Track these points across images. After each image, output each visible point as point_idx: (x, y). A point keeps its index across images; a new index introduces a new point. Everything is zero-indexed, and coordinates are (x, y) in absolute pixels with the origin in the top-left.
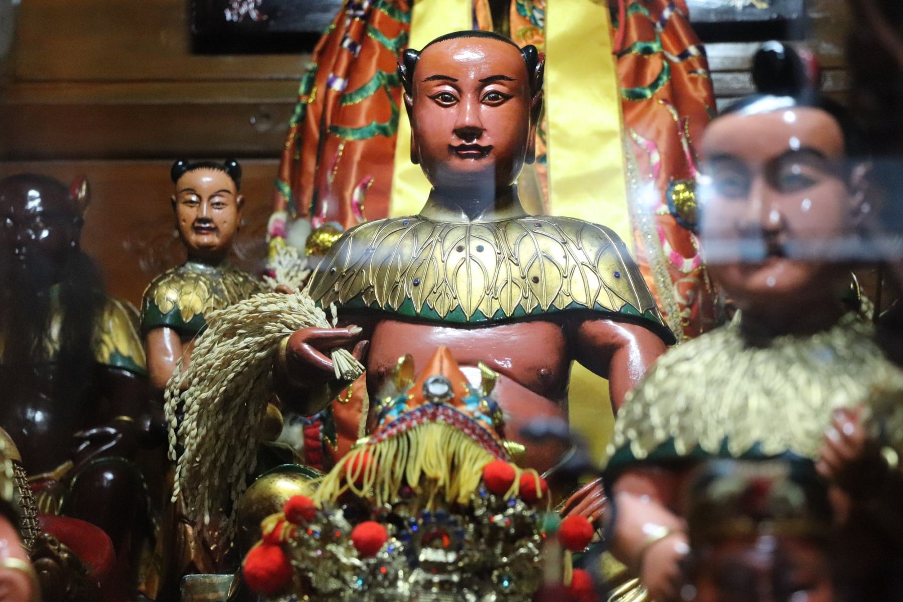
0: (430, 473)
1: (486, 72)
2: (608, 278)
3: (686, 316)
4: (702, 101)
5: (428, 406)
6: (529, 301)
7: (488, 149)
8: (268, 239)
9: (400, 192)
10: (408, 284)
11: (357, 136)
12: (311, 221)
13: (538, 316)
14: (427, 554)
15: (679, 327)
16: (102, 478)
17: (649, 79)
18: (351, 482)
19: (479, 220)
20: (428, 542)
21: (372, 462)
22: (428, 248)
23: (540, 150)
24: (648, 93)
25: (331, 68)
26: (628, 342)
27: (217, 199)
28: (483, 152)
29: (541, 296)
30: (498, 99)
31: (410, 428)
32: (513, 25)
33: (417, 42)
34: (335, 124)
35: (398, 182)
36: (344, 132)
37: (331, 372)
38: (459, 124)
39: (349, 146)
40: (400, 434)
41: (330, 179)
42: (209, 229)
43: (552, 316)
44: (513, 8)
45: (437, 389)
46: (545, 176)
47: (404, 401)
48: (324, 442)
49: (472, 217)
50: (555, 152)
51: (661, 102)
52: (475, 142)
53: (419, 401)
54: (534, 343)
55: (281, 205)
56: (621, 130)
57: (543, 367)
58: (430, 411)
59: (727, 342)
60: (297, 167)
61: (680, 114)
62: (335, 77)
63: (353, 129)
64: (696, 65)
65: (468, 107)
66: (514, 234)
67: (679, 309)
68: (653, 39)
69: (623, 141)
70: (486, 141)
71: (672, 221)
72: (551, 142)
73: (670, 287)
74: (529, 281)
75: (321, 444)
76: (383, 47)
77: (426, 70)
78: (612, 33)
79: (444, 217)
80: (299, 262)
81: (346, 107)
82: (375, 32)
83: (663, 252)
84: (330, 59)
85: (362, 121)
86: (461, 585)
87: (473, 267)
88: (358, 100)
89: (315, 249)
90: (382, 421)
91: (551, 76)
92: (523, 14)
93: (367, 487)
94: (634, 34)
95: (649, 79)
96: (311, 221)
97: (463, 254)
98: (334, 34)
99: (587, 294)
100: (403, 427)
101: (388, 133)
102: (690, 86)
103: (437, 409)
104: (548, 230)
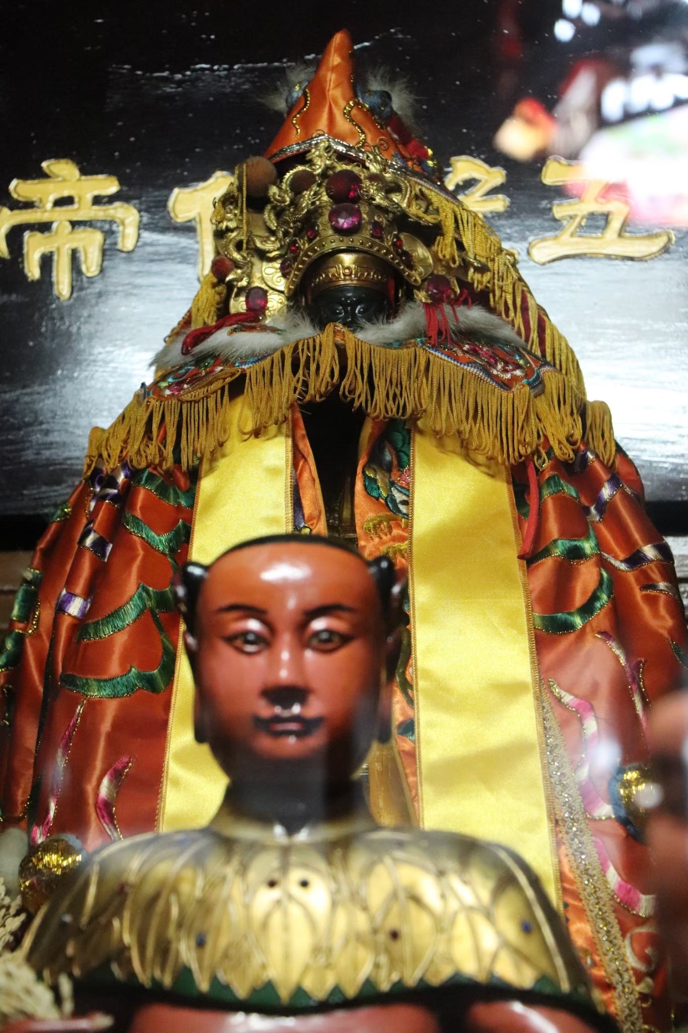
1: (314, 598)
2: (512, 931)
3: (646, 991)
4: (665, 633)
11: (107, 692)
12: (29, 832)
15: (635, 1010)
17: (579, 600)
19: (303, 836)
23: (403, 713)
24: (578, 621)
28: (306, 726)
33: (205, 547)
35: (173, 768)
38: (271, 680)
39: (94, 707)
44: (359, 486)
46: (412, 755)
49: (291, 830)
50: (428, 719)
52: (296, 709)
56: (534, 681)
61: (628, 654)
62: (71, 595)
63: (99, 681)
64: (656, 575)
66: (359, 859)
67: (633, 979)
68: (585, 535)
69: (538, 698)
70: (315, 708)
72: (421, 701)
73: (619, 941)
74: (382, 937)
76: (148, 546)
77: (219, 596)
78: (519, 524)
79: (247, 832)
80: (7, 900)
84: (63, 564)
85: (114, 668)
88: (107, 631)
91: (421, 594)
92: (375, 494)
94: (553, 527)
96: (29, 832)
97: (276, 893)
98: (69, 523)
101: (159, 685)
102: (646, 610)
104: (413, 854)
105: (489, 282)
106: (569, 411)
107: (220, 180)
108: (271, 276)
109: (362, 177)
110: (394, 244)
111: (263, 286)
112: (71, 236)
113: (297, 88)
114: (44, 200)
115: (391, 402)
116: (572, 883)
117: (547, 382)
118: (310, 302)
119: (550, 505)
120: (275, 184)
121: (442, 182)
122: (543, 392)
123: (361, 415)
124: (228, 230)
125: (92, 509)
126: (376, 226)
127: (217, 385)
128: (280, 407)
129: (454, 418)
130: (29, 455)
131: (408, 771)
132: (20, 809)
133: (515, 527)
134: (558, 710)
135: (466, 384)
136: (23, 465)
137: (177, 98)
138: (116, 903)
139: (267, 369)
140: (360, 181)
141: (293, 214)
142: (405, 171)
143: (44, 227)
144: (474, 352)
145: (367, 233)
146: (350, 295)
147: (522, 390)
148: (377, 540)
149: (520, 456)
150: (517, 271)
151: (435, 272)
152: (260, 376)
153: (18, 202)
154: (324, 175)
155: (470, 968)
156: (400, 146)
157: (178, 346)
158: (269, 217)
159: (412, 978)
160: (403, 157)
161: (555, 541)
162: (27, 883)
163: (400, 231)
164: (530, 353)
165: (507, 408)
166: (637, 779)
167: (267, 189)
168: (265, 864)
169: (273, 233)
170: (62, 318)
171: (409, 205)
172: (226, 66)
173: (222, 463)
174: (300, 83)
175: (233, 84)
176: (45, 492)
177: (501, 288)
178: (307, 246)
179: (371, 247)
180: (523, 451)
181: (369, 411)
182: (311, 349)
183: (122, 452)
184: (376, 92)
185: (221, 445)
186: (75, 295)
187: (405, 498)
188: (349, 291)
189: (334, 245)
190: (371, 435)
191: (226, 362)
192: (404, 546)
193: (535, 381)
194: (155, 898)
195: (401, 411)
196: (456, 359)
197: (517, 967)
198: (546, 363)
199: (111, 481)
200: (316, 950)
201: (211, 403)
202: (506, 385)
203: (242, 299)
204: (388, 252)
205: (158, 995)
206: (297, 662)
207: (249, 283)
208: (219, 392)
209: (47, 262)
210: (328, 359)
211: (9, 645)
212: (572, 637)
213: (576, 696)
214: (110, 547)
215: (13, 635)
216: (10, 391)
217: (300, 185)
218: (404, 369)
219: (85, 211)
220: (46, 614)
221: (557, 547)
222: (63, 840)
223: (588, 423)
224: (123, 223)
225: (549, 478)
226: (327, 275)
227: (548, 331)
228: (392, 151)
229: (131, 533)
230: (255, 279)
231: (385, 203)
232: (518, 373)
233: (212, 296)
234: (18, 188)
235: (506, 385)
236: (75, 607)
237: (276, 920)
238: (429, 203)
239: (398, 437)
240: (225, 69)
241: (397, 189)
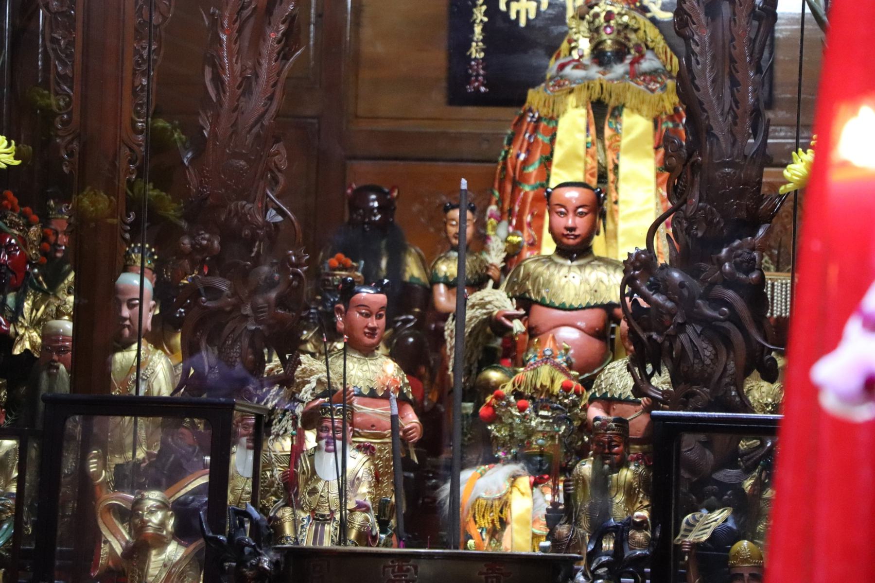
0: (544, 384)
1: (578, 204)
8: (487, 219)
9: (555, 174)
13: (596, 306)
14: (542, 413)
16: (407, 341)
18: (517, 386)
20: (543, 408)
21: (524, 379)
28: (576, 237)
39: (526, 194)
40: (535, 369)
41: (517, 208)
45: (548, 353)
47: (535, 356)
70: (577, 233)
77: (554, 200)
78: (655, 136)
79: (560, 260)
86: (552, 423)
93: (522, 388)
123: (607, 106)
145: (615, 33)
147: (658, 92)
159: (599, 303)
168: (564, 271)
194: (537, 277)
200: (576, 295)
205: (536, 302)
206: (574, 221)
209: (518, 13)
232: (658, 85)
235: (653, 91)
237: (566, 286)
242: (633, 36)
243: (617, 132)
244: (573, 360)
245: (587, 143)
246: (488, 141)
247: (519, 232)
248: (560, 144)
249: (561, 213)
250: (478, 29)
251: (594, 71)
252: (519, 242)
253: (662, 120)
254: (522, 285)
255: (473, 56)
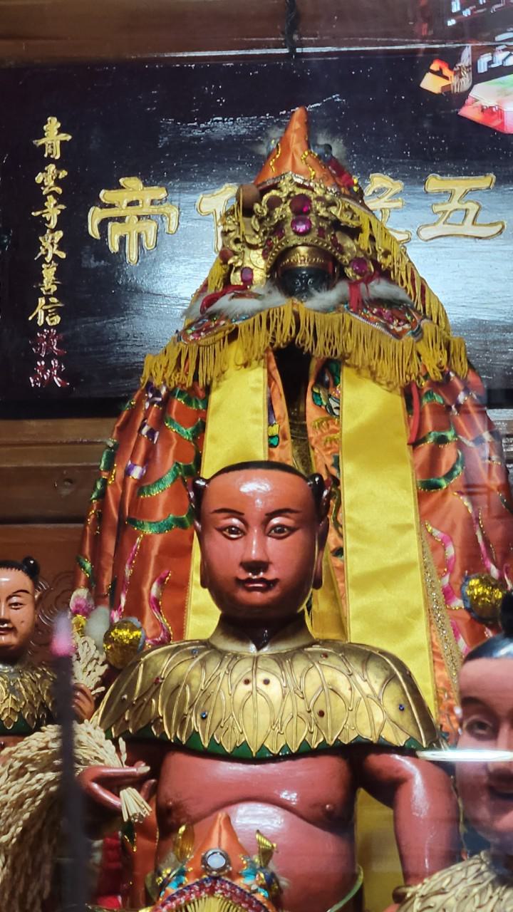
2: (392, 710)
5: (206, 880)
6: (314, 736)
7: (275, 582)
10: (196, 716)
13: (324, 750)
17: (444, 469)
19: (266, 650)
22: (216, 680)
25: (130, 454)
26: (412, 777)
27: (15, 600)
28: (269, 584)
29: (326, 731)
30: (283, 532)
31: (188, 902)
32: (308, 407)
34: (133, 517)
36: (142, 526)
37: (117, 812)
38: (246, 558)
39: (147, 539)
41: (128, 572)
42: (7, 629)
43: (338, 750)
44: (309, 399)
45: (216, 862)
46: (342, 569)
47: (182, 873)
48: (123, 840)
51: (456, 494)
53: (198, 874)
54: (323, 777)
55: (82, 582)
57: (328, 804)
58: (208, 885)
59: (479, 873)
60: (97, 542)
63: (150, 523)
65: (254, 543)
68: (448, 428)
69: (420, 534)
70: (272, 574)
71: (467, 616)
72: (348, 536)
75: (119, 842)
76: (180, 437)
77: (214, 502)
79: (232, 646)
81: (142, 500)
82: (172, 421)
83: (458, 648)
84: (129, 441)
85: (159, 515)
87: (260, 698)
88: (155, 492)
89: (113, 645)
90: (163, 893)
94: (429, 423)
95: (444, 469)
97: (249, 687)
99: (373, 728)
100: (183, 900)
103: (216, 883)
104: (334, 660)
105: (390, 264)
106: (439, 347)
107: (229, 189)
108: (257, 262)
109: (312, 199)
110: (331, 240)
111: (251, 266)
112: (137, 225)
113: (273, 142)
114: (121, 203)
115: (327, 347)
116: (437, 648)
117: (425, 331)
118: (280, 275)
119: (427, 410)
120: (257, 202)
121: (363, 201)
122: (422, 337)
123: (309, 356)
124: (229, 231)
125: (147, 407)
126: (321, 229)
127: (220, 335)
128: (259, 349)
129: (366, 358)
130: (112, 360)
131: (338, 580)
132: (105, 589)
133: (406, 424)
134: (431, 540)
135: (374, 335)
136: (109, 367)
137: (202, 139)
138: (154, 689)
139: (251, 326)
140: (311, 201)
141: (269, 222)
142: (340, 194)
143: (121, 219)
144: (380, 314)
145: (315, 233)
146: (304, 272)
147: (408, 339)
148: (319, 433)
149: (407, 382)
150: (407, 256)
151: (358, 256)
152: (247, 329)
153: (105, 204)
154: (288, 197)
155: (368, 734)
156: (337, 179)
157: (199, 305)
158: (254, 222)
160: (339, 186)
161: (430, 433)
162: (109, 647)
163: (335, 231)
164: (415, 310)
165: (399, 351)
166: (478, 585)
167: (253, 205)
168: (243, 668)
169: (257, 233)
170: (132, 276)
171: (341, 214)
172: (232, 119)
173: (224, 384)
174: (275, 139)
175: (236, 129)
176: (122, 383)
177: (398, 269)
178: (277, 242)
179: (317, 242)
180: (408, 379)
181: (314, 353)
182: (278, 314)
183: (164, 375)
184: (322, 146)
185: (223, 372)
186: (140, 261)
187: (337, 405)
188: (304, 270)
189: (294, 242)
190: (316, 366)
191: (227, 318)
192: (336, 436)
193: (417, 331)
195: (334, 353)
196: (368, 320)
197: (395, 732)
198: (425, 317)
199: (157, 393)
201: (217, 346)
202: (398, 336)
203: (238, 274)
204: (328, 246)
205: (178, 747)
206: (263, 546)
207: (243, 264)
208: (222, 340)
209: (122, 241)
210: (288, 320)
211: (99, 486)
212: (440, 492)
213: (442, 532)
214: (157, 434)
215: (101, 480)
216: (100, 321)
217: (274, 203)
218: (336, 327)
219: (146, 209)
220: (118, 472)
221: (430, 437)
222: (130, 622)
223: (451, 352)
224: (169, 216)
225: (426, 393)
226: (290, 261)
227: (427, 293)
228: (331, 181)
229: (169, 429)
230: (245, 261)
231: (326, 215)
232: (407, 326)
233: (221, 271)
234: (105, 195)
235: (398, 336)
236: (137, 473)
238: (354, 213)
239: (334, 367)
240: (231, 121)
241: (334, 204)
242: (348, 243)
243: (331, 414)
244: (284, 882)
245: (271, 437)
246: (70, 481)
247: (135, 620)
248: (214, 439)
249: (232, 529)
250: (49, 273)
251: (278, 300)
252: (137, 639)
253: (420, 390)
254: (141, 706)
255: (40, 323)
